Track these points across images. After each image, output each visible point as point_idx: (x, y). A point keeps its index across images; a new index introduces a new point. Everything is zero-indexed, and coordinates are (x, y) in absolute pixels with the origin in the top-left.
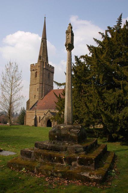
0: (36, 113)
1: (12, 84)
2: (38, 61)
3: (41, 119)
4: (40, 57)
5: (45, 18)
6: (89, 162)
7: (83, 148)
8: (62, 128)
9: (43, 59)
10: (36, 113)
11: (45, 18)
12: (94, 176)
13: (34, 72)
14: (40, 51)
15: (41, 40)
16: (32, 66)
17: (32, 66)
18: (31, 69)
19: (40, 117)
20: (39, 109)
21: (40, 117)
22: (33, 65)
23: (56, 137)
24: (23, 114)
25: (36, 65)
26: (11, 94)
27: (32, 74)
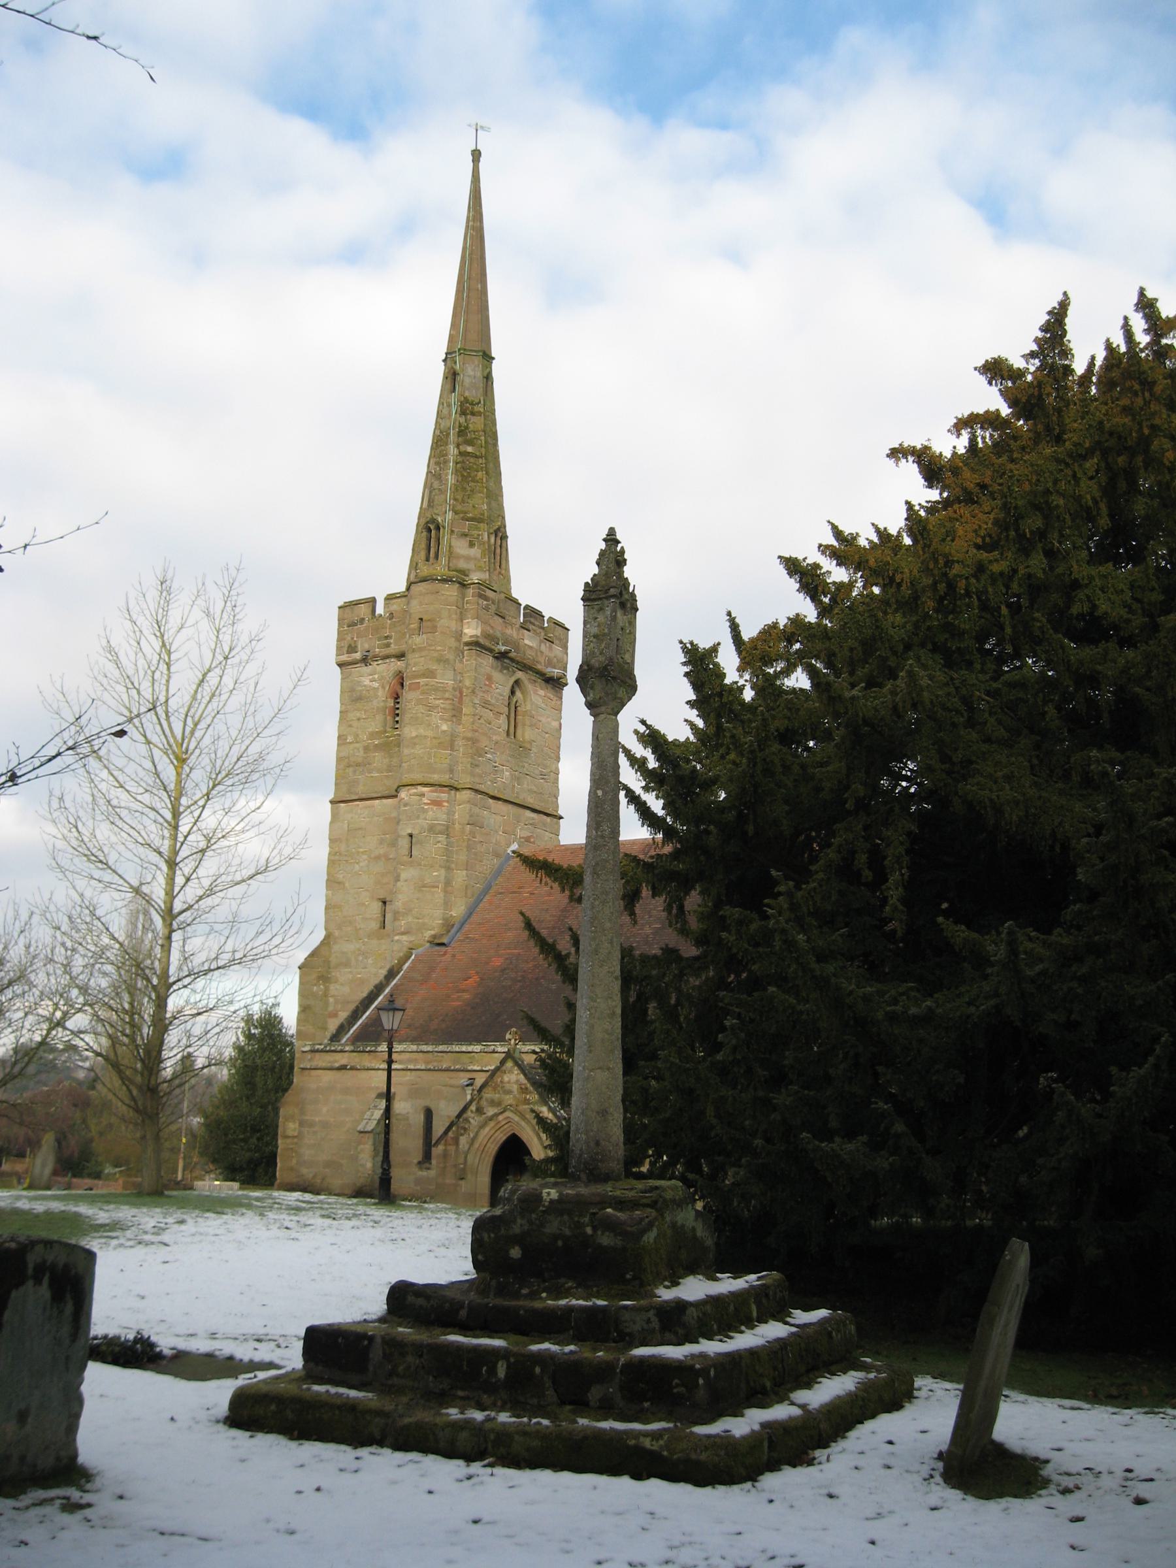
0: (389, 1070)
1: (176, 814)
2: (414, 566)
3: (438, 1129)
4: (430, 531)
5: (476, 155)
6: (677, 1385)
7: (657, 1315)
8: (552, 1201)
9: (461, 547)
10: (389, 1070)
11: (476, 155)
12: (361, 1156)
13: (376, 678)
14: (434, 477)
15: (440, 369)
16: (355, 616)
17: (355, 616)
18: (346, 646)
19: (429, 1114)
20: (422, 1035)
21: (429, 1114)
22: (364, 610)
23: (515, 1253)
24: (267, 1059)
25: (395, 606)
26: (171, 895)
27: (352, 697)
